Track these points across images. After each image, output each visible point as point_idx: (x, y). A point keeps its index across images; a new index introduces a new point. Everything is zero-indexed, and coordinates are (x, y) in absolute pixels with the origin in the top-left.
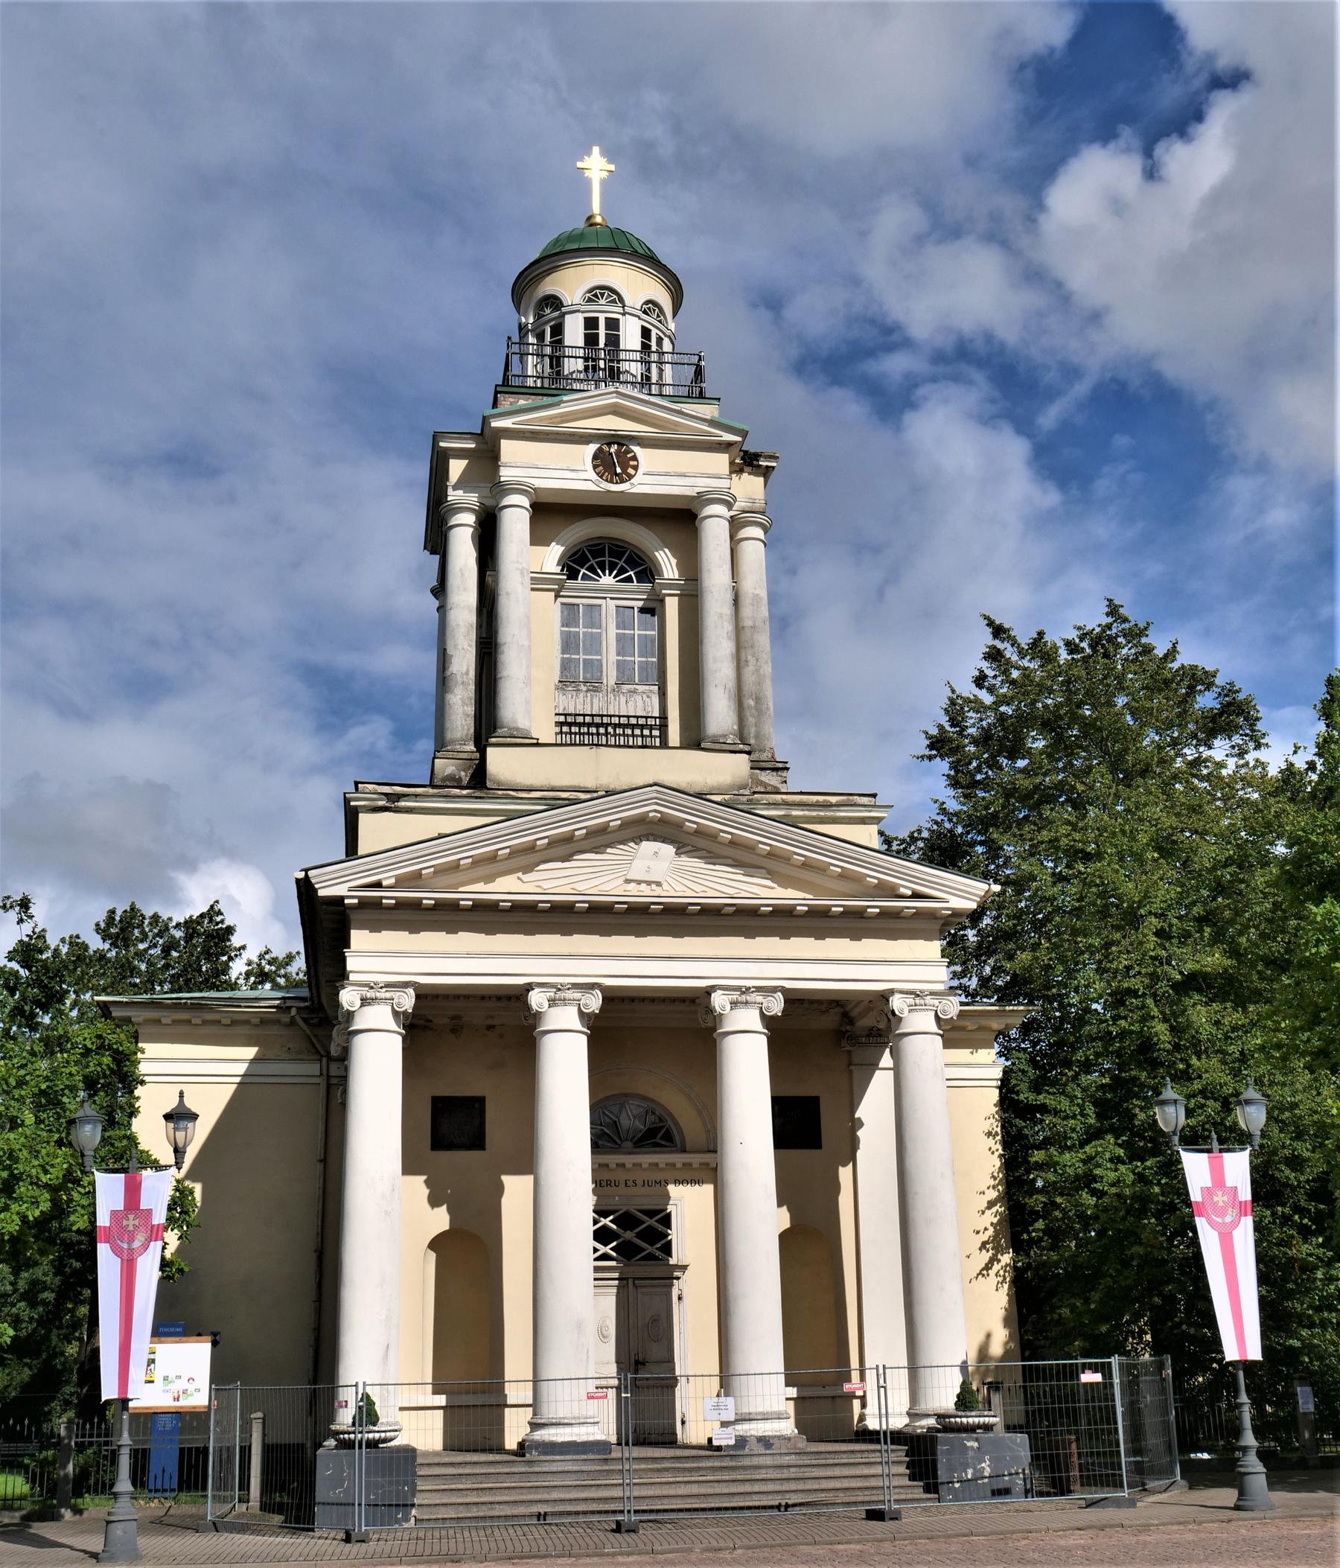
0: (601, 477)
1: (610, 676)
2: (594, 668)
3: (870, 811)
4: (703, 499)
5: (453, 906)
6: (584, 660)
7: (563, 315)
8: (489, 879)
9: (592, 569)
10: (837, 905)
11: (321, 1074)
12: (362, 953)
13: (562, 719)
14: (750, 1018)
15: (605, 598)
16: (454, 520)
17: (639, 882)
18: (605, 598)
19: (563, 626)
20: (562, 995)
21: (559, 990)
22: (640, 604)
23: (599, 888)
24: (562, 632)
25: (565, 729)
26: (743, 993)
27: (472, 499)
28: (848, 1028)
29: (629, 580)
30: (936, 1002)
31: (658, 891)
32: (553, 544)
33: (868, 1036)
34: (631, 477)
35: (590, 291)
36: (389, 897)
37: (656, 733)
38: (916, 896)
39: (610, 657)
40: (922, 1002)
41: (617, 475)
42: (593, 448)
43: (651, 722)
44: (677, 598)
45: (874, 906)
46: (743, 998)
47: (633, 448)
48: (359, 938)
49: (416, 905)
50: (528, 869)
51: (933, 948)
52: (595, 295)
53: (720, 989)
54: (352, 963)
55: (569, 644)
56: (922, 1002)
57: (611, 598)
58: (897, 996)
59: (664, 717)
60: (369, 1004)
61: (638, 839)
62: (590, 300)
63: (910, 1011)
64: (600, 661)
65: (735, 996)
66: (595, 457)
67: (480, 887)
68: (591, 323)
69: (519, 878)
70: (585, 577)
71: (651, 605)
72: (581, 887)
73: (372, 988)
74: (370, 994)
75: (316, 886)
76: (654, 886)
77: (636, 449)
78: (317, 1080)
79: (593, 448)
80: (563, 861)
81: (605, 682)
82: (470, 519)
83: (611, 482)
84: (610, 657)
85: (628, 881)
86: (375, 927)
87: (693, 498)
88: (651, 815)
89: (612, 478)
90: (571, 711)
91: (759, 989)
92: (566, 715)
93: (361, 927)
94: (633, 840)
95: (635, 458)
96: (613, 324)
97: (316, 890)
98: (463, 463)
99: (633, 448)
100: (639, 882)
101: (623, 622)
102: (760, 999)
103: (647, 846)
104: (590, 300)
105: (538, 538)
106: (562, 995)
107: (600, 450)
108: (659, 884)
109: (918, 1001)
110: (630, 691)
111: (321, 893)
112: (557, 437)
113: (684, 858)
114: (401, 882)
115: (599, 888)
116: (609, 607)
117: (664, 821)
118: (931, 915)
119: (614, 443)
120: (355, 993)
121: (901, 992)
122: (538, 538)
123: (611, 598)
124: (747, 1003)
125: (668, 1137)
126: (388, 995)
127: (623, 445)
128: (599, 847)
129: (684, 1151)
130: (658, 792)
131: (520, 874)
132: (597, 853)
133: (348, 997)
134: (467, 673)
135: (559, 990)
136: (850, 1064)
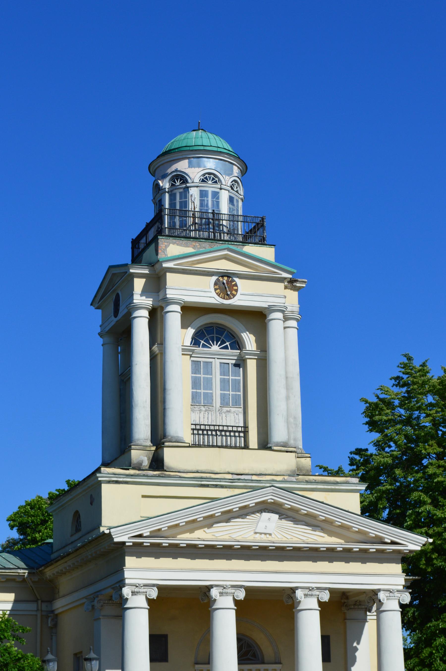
0: (219, 296)
1: (217, 402)
2: (209, 398)
3: (356, 486)
4: (271, 309)
5: (176, 546)
6: (204, 393)
7: (188, 188)
8: (192, 531)
9: (207, 341)
10: (356, 547)
11: (37, 610)
12: (132, 569)
13: (193, 427)
14: (313, 603)
15: (214, 358)
16: (137, 314)
17: (261, 534)
18: (214, 358)
19: (192, 374)
20: (225, 591)
21: (225, 588)
22: (234, 362)
23: (242, 536)
24: (192, 377)
25: (196, 432)
26: (310, 590)
27: (149, 302)
28: (346, 601)
29: (226, 348)
30: (399, 595)
31: (270, 538)
32: (189, 328)
33: (355, 605)
34: (234, 296)
35: (204, 175)
36: (147, 542)
37: (242, 435)
38: (393, 543)
39: (217, 392)
40: (393, 595)
41: (228, 295)
42: (214, 278)
43: (240, 429)
44: (256, 360)
45: (373, 548)
46: (310, 593)
47: (235, 279)
48: (130, 561)
49: (159, 545)
50: (210, 526)
51: (397, 568)
52: (206, 178)
53: (300, 588)
54: (127, 574)
55: (196, 383)
56: (393, 595)
57: (218, 358)
58: (382, 592)
59: (246, 427)
60: (135, 595)
61: (261, 511)
62: (203, 181)
63: (387, 599)
64: (212, 393)
65: (306, 592)
66: (216, 284)
67: (187, 536)
68: (203, 194)
69: (204, 531)
70: (204, 346)
71: (238, 363)
72: (234, 536)
73: (137, 587)
74: (137, 590)
75: (114, 537)
76: (268, 535)
77: (236, 280)
78: (34, 613)
79: (214, 278)
80: (227, 522)
81: (214, 405)
82: (145, 313)
83: (224, 298)
84: (217, 392)
85: (256, 533)
86: (139, 556)
87: (266, 308)
88: (269, 501)
89: (224, 296)
90: (197, 422)
91: (318, 588)
92: (196, 425)
93: (131, 555)
94: (258, 512)
95: (236, 285)
96: (216, 195)
97: (113, 539)
98: (143, 281)
99: (235, 279)
100: (261, 534)
101: (224, 372)
102: (317, 593)
103: (265, 515)
104: (203, 181)
105: (184, 326)
106: (225, 591)
107: (218, 279)
108: (270, 534)
109: (391, 594)
110: (227, 411)
111: (116, 540)
112: (196, 272)
113: (284, 521)
114: (153, 535)
115: (242, 536)
116: (216, 363)
117: (275, 503)
118: (399, 552)
119: (225, 276)
120: (129, 589)
121: (384, 590)
122: (184, 326)
123: (218, 358)
124: (312, 595)
125: (254, 655)
126: (145, 590)
127: (230, 277)
128: (242, 515)
129: (263, 663)
130: (273, 490)
131: (206, 529)
132: (242, 518)
133: (126, 591)
134: (146, 402)
135: (225, 588)
136: (345, 619)
